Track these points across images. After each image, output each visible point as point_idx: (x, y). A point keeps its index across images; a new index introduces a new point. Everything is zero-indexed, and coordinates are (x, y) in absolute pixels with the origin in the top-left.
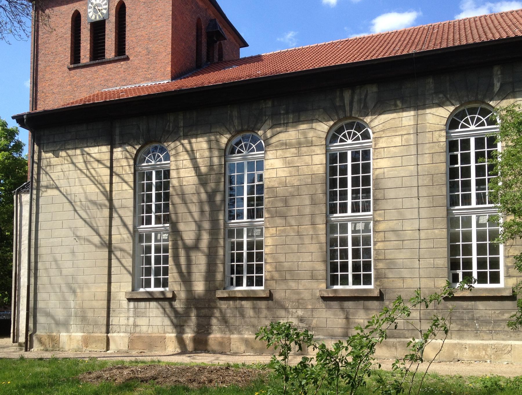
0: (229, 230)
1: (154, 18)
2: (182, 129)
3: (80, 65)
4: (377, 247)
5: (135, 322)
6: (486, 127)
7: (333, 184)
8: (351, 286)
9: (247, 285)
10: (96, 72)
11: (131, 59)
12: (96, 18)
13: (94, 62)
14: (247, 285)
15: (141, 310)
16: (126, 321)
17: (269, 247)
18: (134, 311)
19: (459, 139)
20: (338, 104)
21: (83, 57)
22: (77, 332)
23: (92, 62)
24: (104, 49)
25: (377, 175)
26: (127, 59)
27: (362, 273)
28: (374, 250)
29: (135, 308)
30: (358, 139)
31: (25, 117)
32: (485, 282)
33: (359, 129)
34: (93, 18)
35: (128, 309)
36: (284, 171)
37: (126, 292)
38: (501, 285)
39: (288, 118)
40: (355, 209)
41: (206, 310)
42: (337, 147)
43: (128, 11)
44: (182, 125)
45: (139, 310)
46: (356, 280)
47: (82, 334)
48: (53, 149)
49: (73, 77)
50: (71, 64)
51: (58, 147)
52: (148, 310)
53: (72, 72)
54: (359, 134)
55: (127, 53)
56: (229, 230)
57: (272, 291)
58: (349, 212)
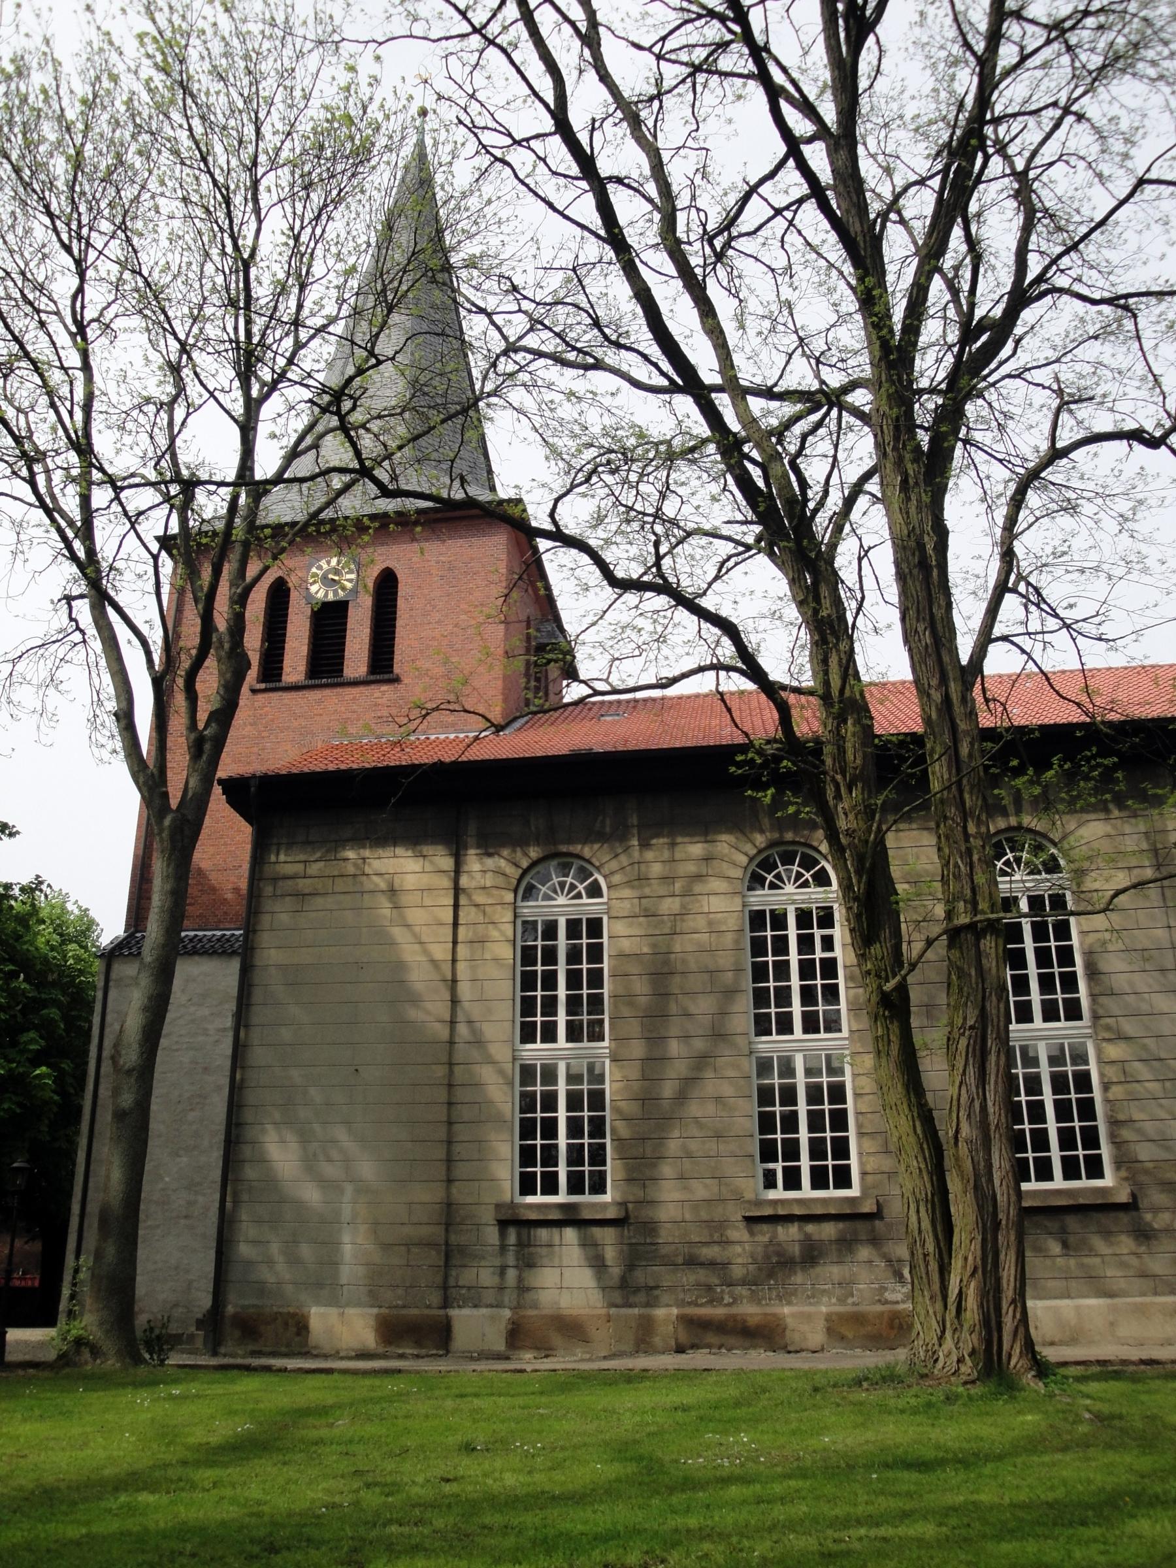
0: (522, 1066)
1: (464, 606)
2: (635, 831)
3: (283, 684)
4: (1111, 1096)
5: (520, 1279)
6: (585, 900)
7: (528, 982)
8: (1059, 1182)
10: (320, 702)
11: (406, 681)
12: (326, 595)
13: (317, 682)
17: (866, 1098)
18: (517, 1252)
19: (540, 920)
23: (372, 678)
24: (343, 657)
25: (1091, 945)
26: (397, 680)
28: (1107, 1101)
30: (579, 896)
31: (252, 782)
32: (826, 1187)
33: (584, 874)
34: (320, 595)
35: (503, 1248)
40: (811, 1025)
42: (533, 909)
43: (403, 590)
44: (635, 822)
47: (375, 1311)
48: (302, 857)
49: (262, 708)
50: (259, 682)
51: (318, 855)
53: (260, 696)
55: (397, 669)
56: (522, 1066)
57: (881, 1199)
58: (1038, 1021)
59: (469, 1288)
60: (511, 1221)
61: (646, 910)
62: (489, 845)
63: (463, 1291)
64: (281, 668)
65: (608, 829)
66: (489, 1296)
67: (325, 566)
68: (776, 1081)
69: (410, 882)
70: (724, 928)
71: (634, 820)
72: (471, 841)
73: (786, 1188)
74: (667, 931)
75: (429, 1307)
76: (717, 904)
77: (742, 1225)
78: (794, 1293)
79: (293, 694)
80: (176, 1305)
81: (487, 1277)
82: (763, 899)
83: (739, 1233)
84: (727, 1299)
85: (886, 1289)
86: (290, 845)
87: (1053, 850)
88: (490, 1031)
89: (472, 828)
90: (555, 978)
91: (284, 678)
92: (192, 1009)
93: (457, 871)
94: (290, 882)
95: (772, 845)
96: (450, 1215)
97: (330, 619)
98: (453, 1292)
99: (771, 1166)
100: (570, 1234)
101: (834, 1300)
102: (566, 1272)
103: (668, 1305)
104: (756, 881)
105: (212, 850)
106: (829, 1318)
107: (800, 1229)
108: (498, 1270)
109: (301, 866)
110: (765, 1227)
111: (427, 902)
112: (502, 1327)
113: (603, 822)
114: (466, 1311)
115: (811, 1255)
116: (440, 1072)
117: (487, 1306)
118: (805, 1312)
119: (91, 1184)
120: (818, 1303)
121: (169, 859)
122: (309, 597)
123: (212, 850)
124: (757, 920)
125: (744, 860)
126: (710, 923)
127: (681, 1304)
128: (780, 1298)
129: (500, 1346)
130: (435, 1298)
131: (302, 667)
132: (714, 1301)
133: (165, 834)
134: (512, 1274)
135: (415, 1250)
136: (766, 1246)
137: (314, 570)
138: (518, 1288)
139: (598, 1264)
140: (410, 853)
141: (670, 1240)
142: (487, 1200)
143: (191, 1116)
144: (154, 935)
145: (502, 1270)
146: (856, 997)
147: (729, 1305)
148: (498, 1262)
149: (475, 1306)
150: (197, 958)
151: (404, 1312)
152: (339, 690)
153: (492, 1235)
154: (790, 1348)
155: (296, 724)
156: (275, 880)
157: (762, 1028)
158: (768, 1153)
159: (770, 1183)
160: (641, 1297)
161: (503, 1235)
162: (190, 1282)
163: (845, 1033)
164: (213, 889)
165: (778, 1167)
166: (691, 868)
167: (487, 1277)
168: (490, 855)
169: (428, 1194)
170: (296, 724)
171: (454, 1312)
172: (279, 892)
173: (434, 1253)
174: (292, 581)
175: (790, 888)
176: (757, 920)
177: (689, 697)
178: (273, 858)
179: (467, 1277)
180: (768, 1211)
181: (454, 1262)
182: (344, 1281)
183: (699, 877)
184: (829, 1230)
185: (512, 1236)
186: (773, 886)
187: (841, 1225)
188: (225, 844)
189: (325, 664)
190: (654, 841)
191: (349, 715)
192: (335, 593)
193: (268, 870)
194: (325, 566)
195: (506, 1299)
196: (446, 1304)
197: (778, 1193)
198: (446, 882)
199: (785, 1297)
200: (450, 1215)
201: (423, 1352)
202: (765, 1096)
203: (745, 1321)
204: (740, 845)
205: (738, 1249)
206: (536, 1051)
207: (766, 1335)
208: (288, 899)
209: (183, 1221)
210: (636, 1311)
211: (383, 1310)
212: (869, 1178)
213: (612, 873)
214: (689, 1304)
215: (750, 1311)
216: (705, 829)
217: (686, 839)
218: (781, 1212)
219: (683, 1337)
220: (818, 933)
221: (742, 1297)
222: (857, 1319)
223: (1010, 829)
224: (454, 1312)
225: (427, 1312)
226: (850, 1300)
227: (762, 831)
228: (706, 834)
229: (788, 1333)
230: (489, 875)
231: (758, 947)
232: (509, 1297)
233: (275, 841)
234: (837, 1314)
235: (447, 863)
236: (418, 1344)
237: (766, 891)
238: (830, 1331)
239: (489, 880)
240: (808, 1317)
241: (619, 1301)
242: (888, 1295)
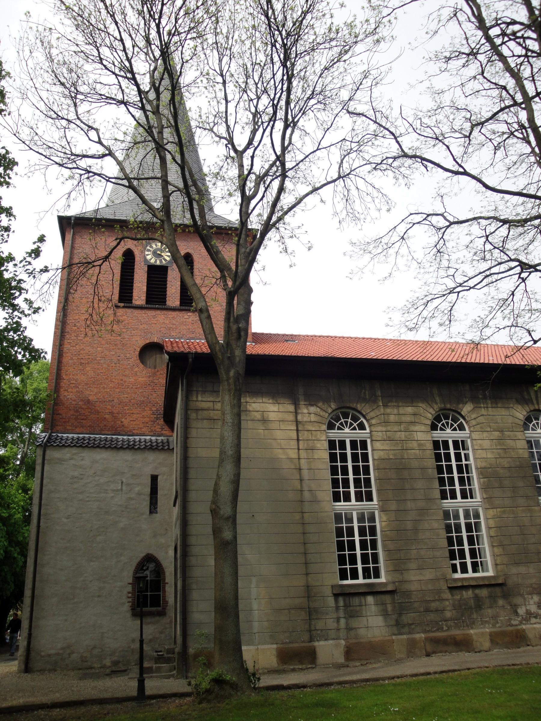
2: (380, 398)
5: (347, 624)
6: (358, 431)
8: (361, 580)
9: (364, 578)
12: (151, 259)
14: (364, 578)
15: (355, 608)
16: (335, 625)
18: (345, 610)
19: (337, 439)
20: (526, 397)
21: (136, 298)
22: (265, 643)
27: (348, 566)
29: (345, 606)
30: (354, 429)
31: (190, 356)
34: (153, 261)
35: (337, 608)
36: (493, 452)
37: (332, 586)
38: (383, 579)
39: (487, 404)
41: (438, 603)
45: (351, 608)
46: (367, 574)
47: (275, 646)
48: (211, 399)
52: (364, 607)
54: (338, 424)
59: (322, 630)
60: (341, 594)
61: (389, 437)
62: (311, 401)
63: (319, 632)
64: (132, 296)
65: (367, 397)
66: (332, 634)
67: (154, 246)
68: (473, 521)
69: (272, 416)
70: (425, 448)
71: (379, 393)
72: (301, 397)
73: (462, 573)
74: (400, 448)
75: (304, 642)
76: (420, 436)
77: (447, 591)
78: (474, 623)
79: (139, 311)
80: (94, 647)
81: (331, 624)
82: (438, 435)
83: (447, 595)
84: (445, 628)
85: (511, 619)
86: (204, 392)
87: (362, 419)
88: (321, 495)
89: (301, 390)
90: (347, 468)
91: (133, 301)
92: (97, 478)
93: (296, 413)
94: (205, 412)
95: (441, 410)
96: (309, 592)
97: (157, 274)
98: (314, 633)
99: (454, 562)
100: (370, 599)
101: (491, 626)
102: (370, 619)
103: (419, 633)
104: (434, 427)
105: (95, 390)
106: (491, 634)
107: (473, 592)
108: (336, 620)
109: (211, 404)
110: (458, 592)
111: (283, 427)
112: (342, 649)
113: (365, 393)
114: (322, 643)
115: (479, 604)
116: (298, 516)
117: (334, 639)
118: (480, 633)
119: (37, 579)
120: (485, 627)
121: (234, 395)
122: (146, 260)
123: (95, 390)
124: (436, 444)
125: (430, 416)
126: (419, 445)
127: (425, 632)
128: (467, 626)
129: (341, 660)
130: (306, 637)
131: (144, 297)
132: (440, 629)
133: (231, 381)
134: (343, 621)
135: (293, 612)
136: (459, 601)
137: (148, 248)
138: (346, 628)
139: (385, 614)
140: (271, 401)
141: (417, 600)
142: (326, 584)
143: (99, 539)
144: (230, 439)
145: (338, 620)
146: (484, 482)
147: (446, 631)
148: (335, 616)
149: (326, 640)
150: (98, 450)
151: (291, 645)
152: (165, 312)
153: (331, 601)
154: (476, 650)
155: (141, 327)
156: (197, 410)
157: (444, 496)
158: (452, 556)
159: (455, 570)
160: (406, 630)
161: (336, 601)
162: (103, 633)
163: (479, 499)
164: (98, 412)
165: (457, 562)
166: (408, 419)
167: (331, 624)
168: (312, 405)
169: (300, 582)
170: (141, 327)
171: (316, 644)
172: (200, 417)
173: (303, 613)
174: (137, 253)
175: (449, 431)
176: (436, 444)
177: (296, 336)
178: (195, 399)
179: (320, 625)
180: (460, 584)
181: (313, 617)
182: (255, 630)
183: (413, 423)
184: (484, 593)
185: (341, 603)
186: (339, 428)
187: (489, 590)
188: (104, 388)
189: (156, 297)
190: (389, 404)
191: (171, 326)
192: (161, 261)
193: (192, 405)
194: (154, 246)
195: (341, 635)
196: (311, 640)
197: (459, 575)
198: (291, 417)
199: (472, 625)
200: (309, 592)
201: (304, 666)
202: (448, 528)
203: (455, 638)
204: (428, 409)
205: (447, 603)
206: (341, 506)
207: (464, 644)
208: (205, 421)
209: (96, 599)
210: (405, 637)
211: (279, 646)
212: (499, 567)
213: (372, 418)
214: (429, 631)
215: (456, 632)
216: (411, 400)
217: (404, 404)
218: (465, 584)
219: (429, 648)
220: (463, 453)
221: (451, 626)
222: (503, 634)
223: (535, 410)
224: (316, 644)
225: (303, 644)
226: (497, 625)
227: (437, 403)
228: (412, 402)
229: (474, 643)
230: (312, 415)
231: (438, 457)
232: (343, 634)
233: (195, 389)
234: (494, 632)
235: (291, 408)
236: (301, 663)
237: (336, 431)
238: (492, 641)
239: (313, 418)
240: (483, 634)
241: (396, 632)
242: (513, 622)
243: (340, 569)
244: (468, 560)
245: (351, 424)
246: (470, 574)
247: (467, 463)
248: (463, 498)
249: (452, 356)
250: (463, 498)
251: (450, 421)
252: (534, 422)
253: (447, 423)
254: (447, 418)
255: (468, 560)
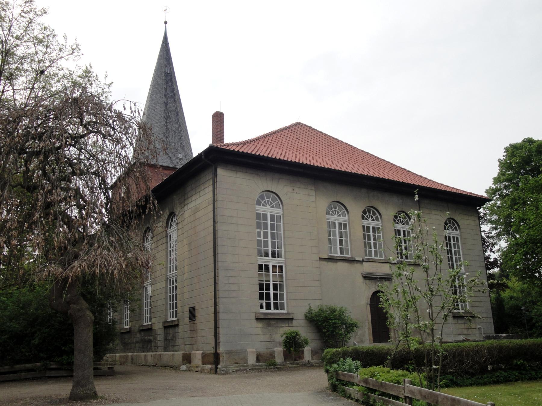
73: (266, 309)
159: (262, 307)
176: (258, 216)
180: (170, 324)
243: (260, 293)
244: (272, 301)
245: (271, 203)
246: (272, 311)
247: (259, 230)
248: (272, 257)
249: (252, 149)
250: (272, 257)
251: (270, 200)
252: (368, 214)
253: (335, 211)
254: (369, 212)
255: (272, 301)
